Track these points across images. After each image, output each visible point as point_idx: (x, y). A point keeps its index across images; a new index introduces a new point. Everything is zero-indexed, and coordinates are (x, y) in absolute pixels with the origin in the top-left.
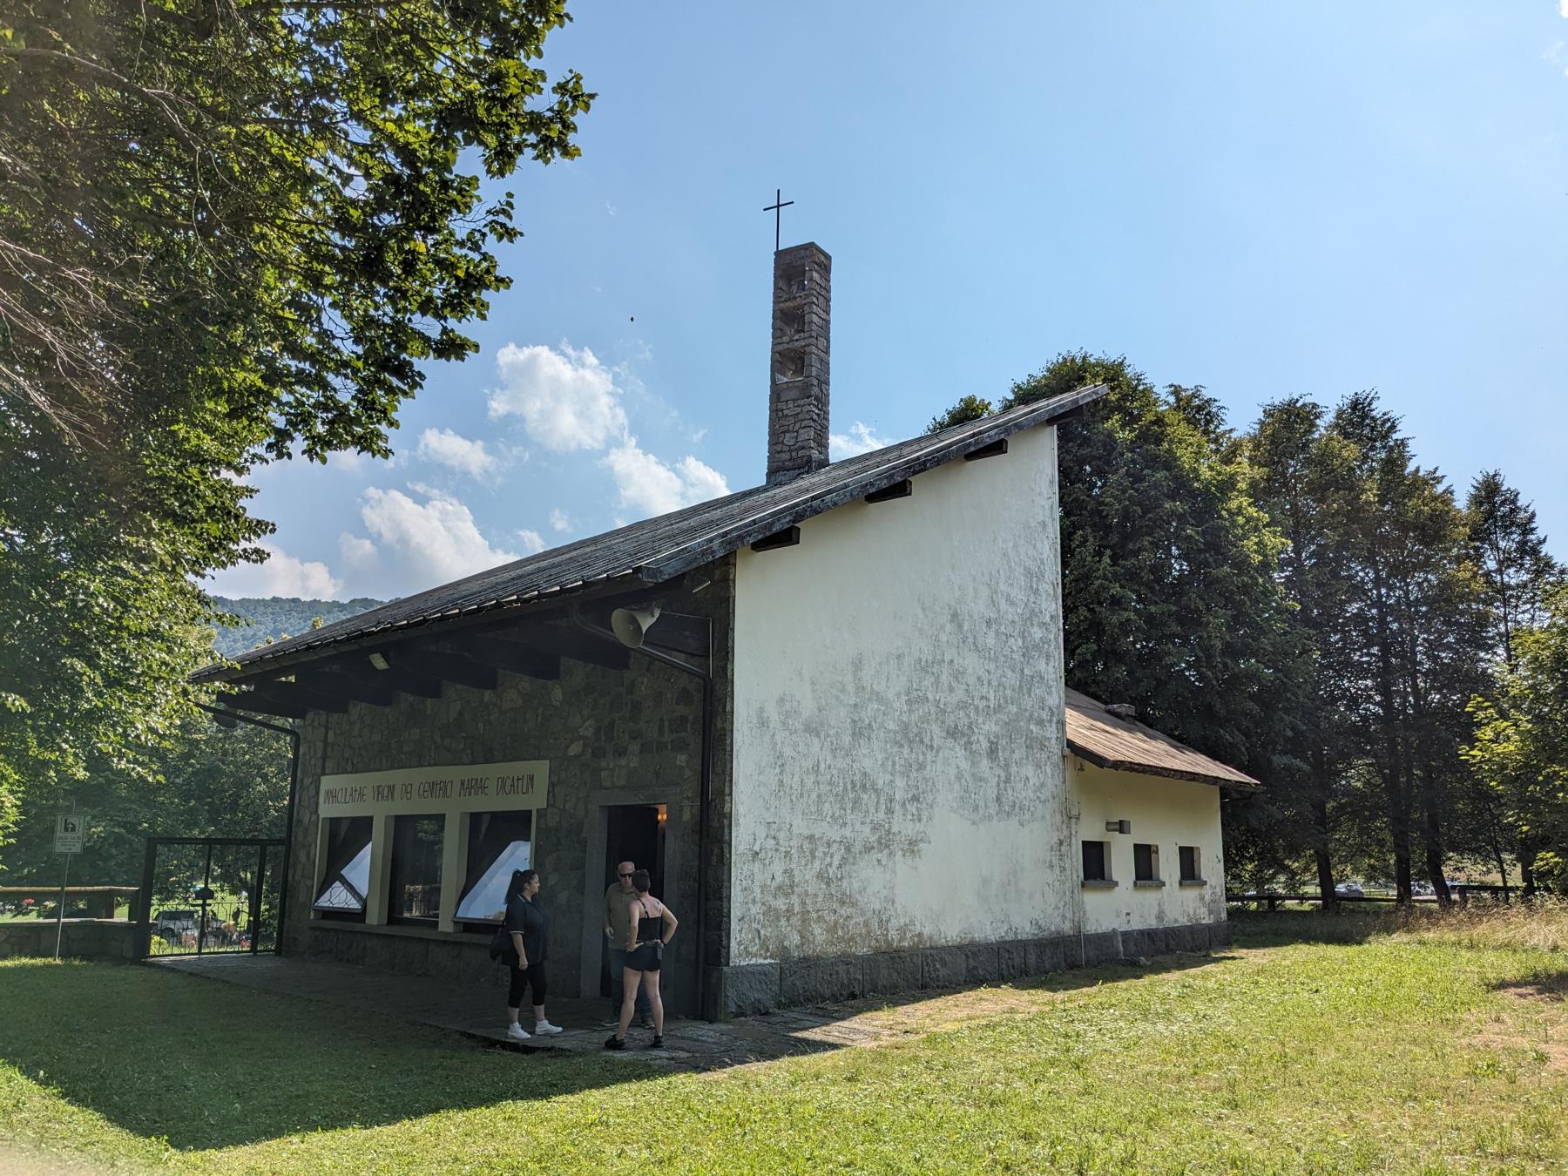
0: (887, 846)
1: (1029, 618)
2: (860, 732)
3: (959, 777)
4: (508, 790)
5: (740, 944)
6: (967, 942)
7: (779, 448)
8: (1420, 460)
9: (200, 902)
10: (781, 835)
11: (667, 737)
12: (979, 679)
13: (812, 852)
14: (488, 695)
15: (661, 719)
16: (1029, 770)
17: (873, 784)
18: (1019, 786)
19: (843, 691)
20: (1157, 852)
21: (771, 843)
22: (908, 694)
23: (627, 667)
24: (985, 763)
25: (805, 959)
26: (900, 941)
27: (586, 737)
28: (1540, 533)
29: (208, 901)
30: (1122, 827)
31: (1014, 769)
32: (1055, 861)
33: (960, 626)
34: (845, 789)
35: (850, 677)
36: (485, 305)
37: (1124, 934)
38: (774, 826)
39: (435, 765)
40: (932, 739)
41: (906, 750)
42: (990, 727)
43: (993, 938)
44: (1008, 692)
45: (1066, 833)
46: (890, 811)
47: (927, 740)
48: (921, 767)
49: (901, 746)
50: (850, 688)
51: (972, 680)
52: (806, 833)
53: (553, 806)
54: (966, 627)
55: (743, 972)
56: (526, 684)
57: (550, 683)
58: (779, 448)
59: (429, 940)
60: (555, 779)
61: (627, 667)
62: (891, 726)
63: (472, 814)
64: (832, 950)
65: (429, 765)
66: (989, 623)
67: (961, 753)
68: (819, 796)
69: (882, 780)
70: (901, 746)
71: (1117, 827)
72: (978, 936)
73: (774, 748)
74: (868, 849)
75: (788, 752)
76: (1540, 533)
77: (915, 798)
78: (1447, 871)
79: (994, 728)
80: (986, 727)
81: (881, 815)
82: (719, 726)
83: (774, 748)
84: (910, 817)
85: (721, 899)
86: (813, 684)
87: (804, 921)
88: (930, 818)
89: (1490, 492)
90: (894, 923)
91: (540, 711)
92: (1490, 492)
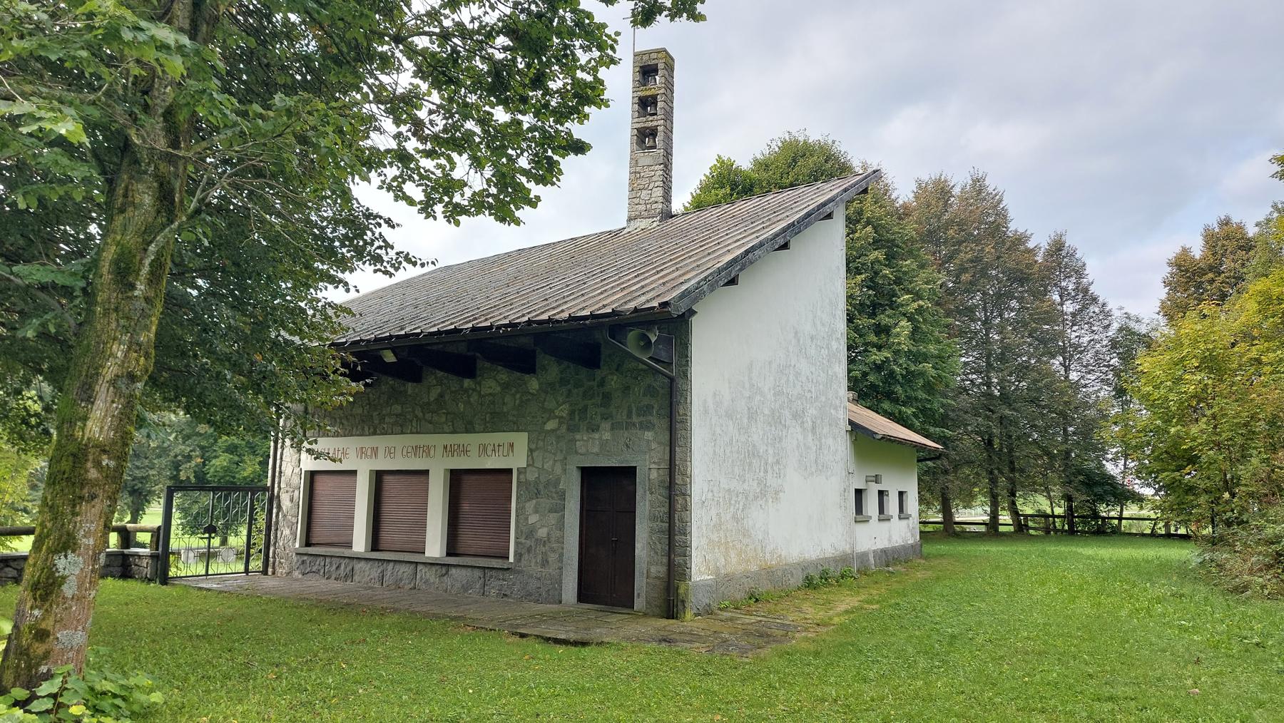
0: (765, 496)
1: (831, 335)
2: (752, 415)
3: (798, 447)
4: (489, 453)
5: (696, 566)
6: (802, 560)
7: (636, 201)
8: (1016, 225)
9: (207, 535)
10: (715, 489)
11: (635, 419)
12: (807, 377)
13: (730, 500)
14: (467, 383)
15: (630, 407)
16: (830, 441)
17: (758, 452)
18: (826, 452)
19: (744, 387)
20: (888, 495)
21: (710, 494)
22: (774, 389)
23: (599, 367)
24: (810, 436)
25: (727, 575)
26: (771, 561)
27: (562, 417)
28: (1090, 278)
29: (213, 535)
30: (877, 479)
31: (823, 440)
32: (842, 504)
33: (799, 341)
34: (745, 457)
35: (746, 378)
36: (586, 116)
37: (874, 551)
38: (712, 483)
39: (417, 433)
40: (785, 421)
41: (773, 428)
42: (812, 411)
43: (814, 557)
44: (821, 387)
45: (847, 483)
46: (766, 472)
47: (783, 422)
48: (781, 439)
49: (771, 426)
50: (747, 385)
51: (804, 379)
52: (727, 487)
53: (532, 465)
54: (801, 342)
55: (697, 585)
56: (504, 375)
57: (527, 377)
58: (636, 201)
59: (417, 563)
60: (533, 446)
61: (599, 367)
62: (766, 412)
63: (451, 470)
64: (741, 568)
65: (412, 433)
66: (812, 338)
67: (799, 429)
68: (733, 461)
69: (762, 449)
70: (771, 426)
71: (874, 479)
72: (807, 556)
73: (711, 429)
74: (756, 498)
75: (718, 431)
76: (1090, 278)
77: (778, 462)
78: (1019, 502)
79: (814, 412)
80: (810, 411)
81: (762, 474)
82: (681, 412)
83: (711, 429)
84: (775, 475)
85: (685, 534)
86: (729, 383)
87: (726, 549)
88: (785, 476)
89: (1057, 247)
90: (769, 549)
91: (518, 396)
92: (1057, 247)
